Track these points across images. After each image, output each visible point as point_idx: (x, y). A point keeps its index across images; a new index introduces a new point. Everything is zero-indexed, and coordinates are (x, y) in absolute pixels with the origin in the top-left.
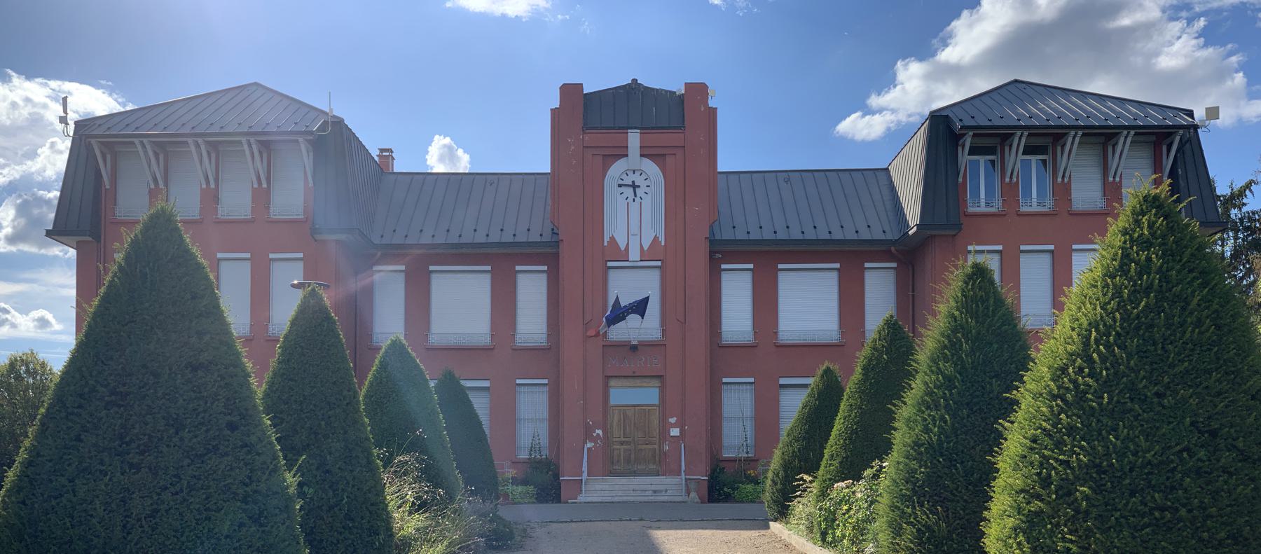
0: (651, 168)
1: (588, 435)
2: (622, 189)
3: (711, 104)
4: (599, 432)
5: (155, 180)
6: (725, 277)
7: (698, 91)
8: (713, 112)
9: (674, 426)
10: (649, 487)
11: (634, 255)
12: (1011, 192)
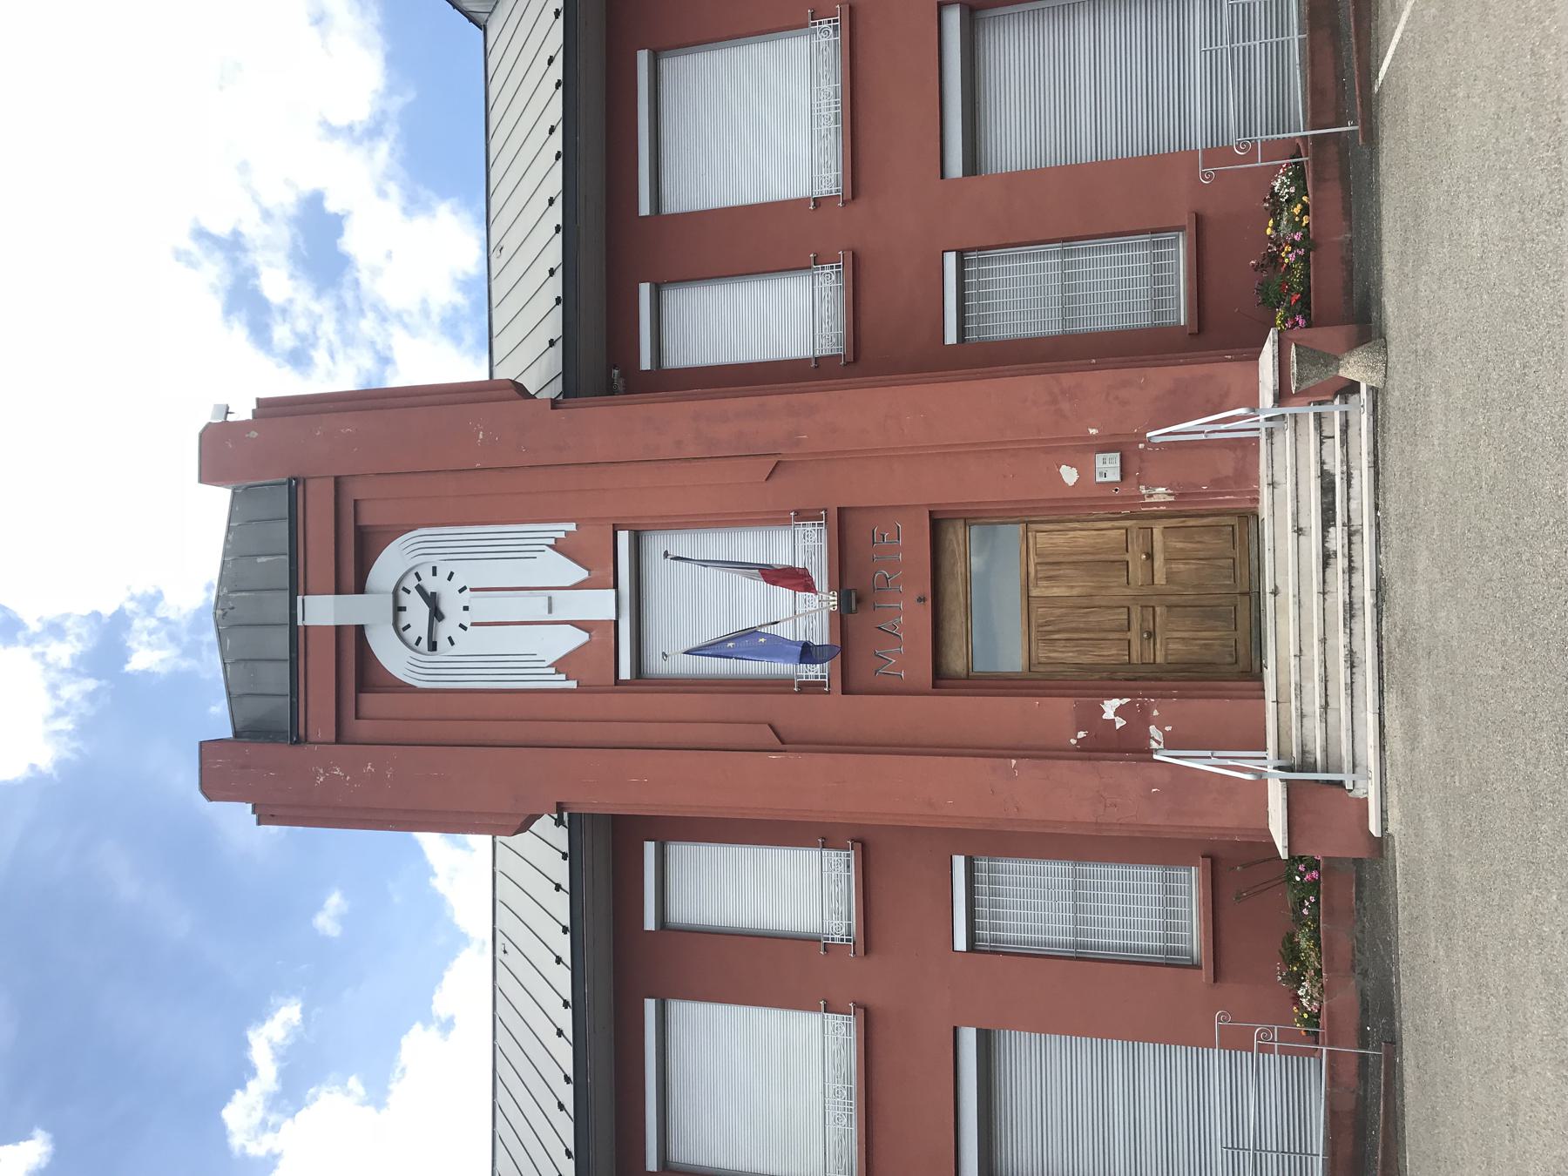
0: (389, 566)
1: (1131, 746)
2: (442, 643)
4: (1110, 707)
6: (676, 358)
9: (1086, 471)
11: (600, 605)
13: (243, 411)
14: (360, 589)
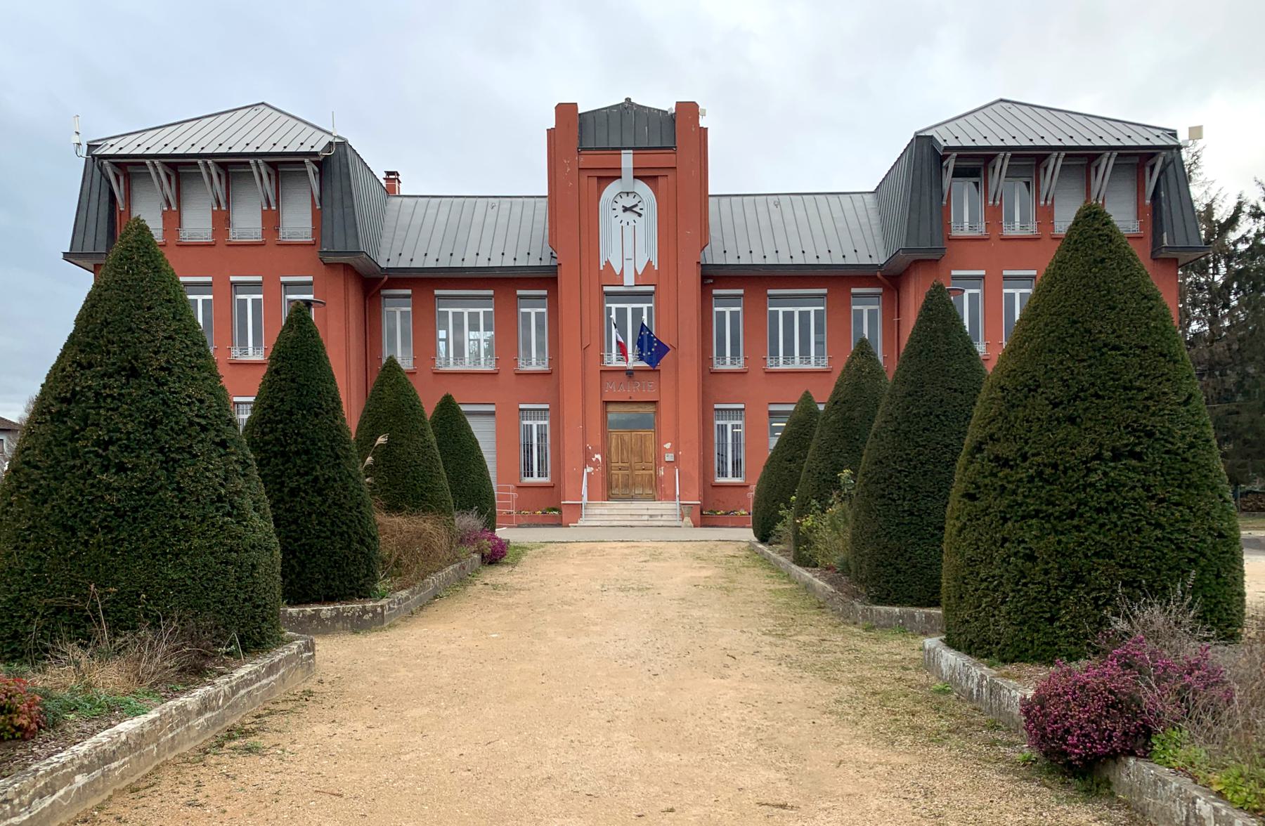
0: (643, 189)
1: (587, 461)
3: (702, 123)
4: (598, 456)
5: (168, 202)
7: (689, 110)
8: (704, 131)
9: (669, 451)
10: (645, 512)
11: (629, 280)
12: (994, 214)
13: (703, 123)
14: (635, 177)
